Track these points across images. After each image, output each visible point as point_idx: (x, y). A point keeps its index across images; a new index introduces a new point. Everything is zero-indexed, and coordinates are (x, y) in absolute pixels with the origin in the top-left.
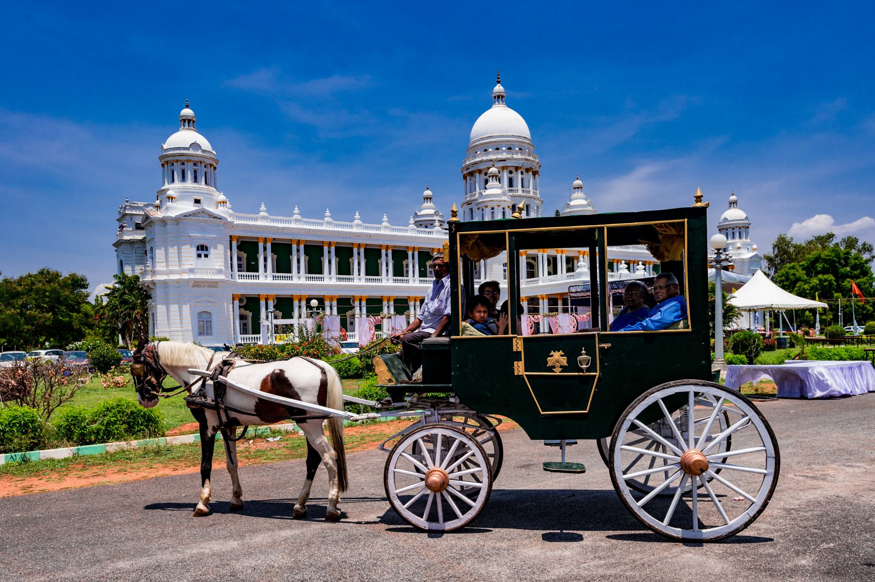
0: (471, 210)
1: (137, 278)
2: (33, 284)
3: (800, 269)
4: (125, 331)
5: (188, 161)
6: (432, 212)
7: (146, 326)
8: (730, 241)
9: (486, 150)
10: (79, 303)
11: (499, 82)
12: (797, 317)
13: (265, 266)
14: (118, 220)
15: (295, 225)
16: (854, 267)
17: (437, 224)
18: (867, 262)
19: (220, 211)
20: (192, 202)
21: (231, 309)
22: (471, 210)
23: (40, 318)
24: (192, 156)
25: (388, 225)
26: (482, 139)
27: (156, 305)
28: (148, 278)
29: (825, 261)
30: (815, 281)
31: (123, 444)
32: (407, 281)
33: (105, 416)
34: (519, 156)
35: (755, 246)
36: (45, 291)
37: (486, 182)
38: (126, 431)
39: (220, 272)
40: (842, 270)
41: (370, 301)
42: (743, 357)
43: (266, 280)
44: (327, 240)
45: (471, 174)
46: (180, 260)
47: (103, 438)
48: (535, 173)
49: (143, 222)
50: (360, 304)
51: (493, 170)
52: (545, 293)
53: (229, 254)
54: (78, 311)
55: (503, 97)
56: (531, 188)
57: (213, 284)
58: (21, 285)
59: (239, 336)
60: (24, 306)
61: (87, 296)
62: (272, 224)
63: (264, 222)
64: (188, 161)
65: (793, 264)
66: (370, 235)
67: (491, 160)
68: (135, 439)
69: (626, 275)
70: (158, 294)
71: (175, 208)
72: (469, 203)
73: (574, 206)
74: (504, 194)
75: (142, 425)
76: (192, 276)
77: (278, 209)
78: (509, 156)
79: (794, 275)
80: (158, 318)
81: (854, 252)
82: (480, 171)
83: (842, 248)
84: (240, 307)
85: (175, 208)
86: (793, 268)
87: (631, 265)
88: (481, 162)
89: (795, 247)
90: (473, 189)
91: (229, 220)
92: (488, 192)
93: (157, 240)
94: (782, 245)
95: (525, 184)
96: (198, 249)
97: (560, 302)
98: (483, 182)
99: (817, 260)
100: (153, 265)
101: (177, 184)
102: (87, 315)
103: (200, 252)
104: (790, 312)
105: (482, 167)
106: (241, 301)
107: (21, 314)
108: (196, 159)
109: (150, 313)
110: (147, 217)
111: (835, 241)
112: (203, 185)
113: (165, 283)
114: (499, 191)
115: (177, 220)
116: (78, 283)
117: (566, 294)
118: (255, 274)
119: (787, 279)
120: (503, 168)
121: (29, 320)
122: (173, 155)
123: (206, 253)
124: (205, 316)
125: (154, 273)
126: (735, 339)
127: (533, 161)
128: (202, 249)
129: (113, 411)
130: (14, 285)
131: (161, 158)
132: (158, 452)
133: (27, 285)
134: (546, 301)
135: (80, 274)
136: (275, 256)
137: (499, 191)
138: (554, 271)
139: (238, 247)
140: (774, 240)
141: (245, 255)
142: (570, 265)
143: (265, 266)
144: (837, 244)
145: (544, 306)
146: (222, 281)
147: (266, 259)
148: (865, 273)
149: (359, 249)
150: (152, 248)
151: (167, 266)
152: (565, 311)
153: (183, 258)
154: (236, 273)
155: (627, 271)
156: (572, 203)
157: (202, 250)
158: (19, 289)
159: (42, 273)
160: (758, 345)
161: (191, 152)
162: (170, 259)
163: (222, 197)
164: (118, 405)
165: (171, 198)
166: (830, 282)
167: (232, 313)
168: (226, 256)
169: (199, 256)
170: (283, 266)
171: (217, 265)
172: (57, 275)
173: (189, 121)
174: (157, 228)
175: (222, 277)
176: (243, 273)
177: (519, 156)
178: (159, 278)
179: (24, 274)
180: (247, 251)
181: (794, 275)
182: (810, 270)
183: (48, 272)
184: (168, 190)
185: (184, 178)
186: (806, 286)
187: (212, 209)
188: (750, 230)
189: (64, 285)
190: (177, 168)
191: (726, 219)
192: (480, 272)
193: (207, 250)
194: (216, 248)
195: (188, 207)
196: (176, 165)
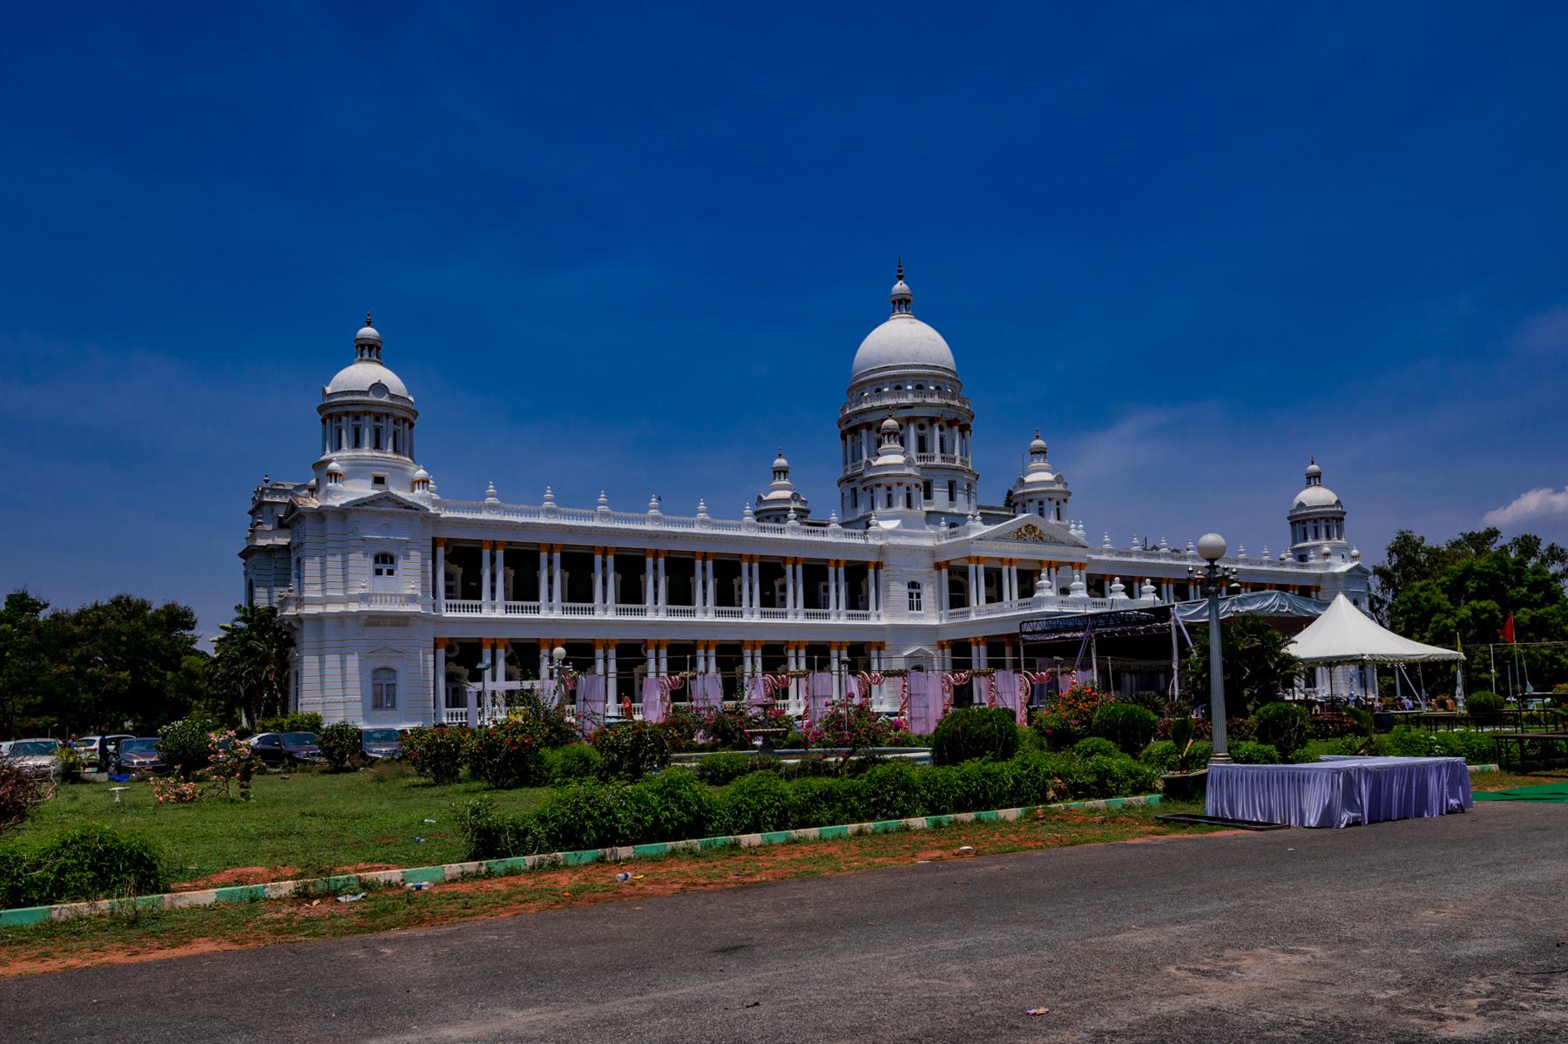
0: (854, 490)
1: (273, 611)
2: (101, 621)
3: (1438, 591)
4: (249, 703)
5: (366, 413)
6: (787, 494)
7: (286, 694)
8: (1310, 543)
9: (878, 390)
10: (178, 656)
11: (900, 278)
12: (1431, 676)
13: (493, 590)
14: (251, 513)
15: (545, 517)
16: (1535, 587)
17: (792, 514)
18: (1555, 578)
19: (417, 496)
20: (370, 482)
21: (431, 664)
22: (854, 490)
23: (109, 680)
24: (372, 404)
25: (497, 501)
26: (873, 371)
27: (301, 657)
28: (291, 611)
29: (1481, 575)
30: (1464, 611)
31: (83, 906)
32: (537, 610)
33: (58, 855)
34: (936, 400)
35: (1355, 552)
36: (120, 633)
37: (879, 443)
38: (92, 883)
39: (412, 599)
40: (1512, 593)
41: (571, 647)
42: (1270, 748)
43: (493, 611)
44: (833, 557)
45: (855, 431)
46: (345, 582)
47: (49, 895)
48: (964, 429)
49: (287, 516)
50: (657, 654)
51: (890, 423)
52: (980, 633)
53: (430, 569)
54: (176, 668)
55: (908, 301)
56: (957, 453)
57: (401, 620)
58: (79, 624)
59: (445, 710)
60: (84, 660)
61: (193, 641)
62: (506, 518)
63: (491, 513)
64: (366, 413)
65: (1424, 582)
66: (675, 536)
67: (887, 407)
68: (107, 897)
69: (1124, 602)
70: (307, 637)
71: (341, 492)
72: (849, 479)
73: (1033, 484)
74: (909, 463)
75: (125, 870)
76: (364, 607)
77: (518, 491)
78: (918, 400)
79: (1428, 600)
80: (306, 680)
81: (1532, 562)
82: (869, 426)
83: (1512, 555)
84: (447, 660)
85: (341, 492)
86: (1423, 589)
87: (1164, 586)
88: (871, 409)
89: (1429, 552)
90: (856, 456)
91: (432, 510)
92: (881, 461)
93: (307, 546)
94: (1405, 547)
95: (947, 446)
96: (377, 561)
97: (1008, 650)
98: (874, 444)
99: (1468, 572)
100: (301, 591)
101: (347, 453)
102: (190, 675)
103: (379, 566)
104: (1411, 666)
105: (871, 418)
106: (449, 649)
107: (78, 674)
108: (380, 410)
109: (292, 671)
110: (292, 508)
111: (1500, 543)
112: (389, 454)
113: (319, 618)
114: (899, 459)
115: (344, 512)
116: (178, 619)
117: (1016, 635)
118: (475, 602)
119: (1416, 608)
120: (909, 420)
121: (93, 683)
122: (342, 404)
123: (389, 566)
124: (385, 675)
125: (300, 602)
126: (1261, 718)
127: (959, 408)
128: (384, 562)
129: (75, 847)
130: (69, 625)
131: (321, 409)
132: (134, 921)
133: (91, 623)
134: (983, 648)
135: (182, 604)
136: (512, 573)
137: (899, 459)
138: (995, 596)
139: (446, 557)
140: (1391, 539)
141: (460, 571)
142: (1027, 586)
143: (493, 590)
144: (1504, 548)
145: (979, 657)
146: (416, 615)
147: (494, 576)
148: (1553, 597)
149: (704, 563)
150: (299, 561)
151: (324, 590)
152: (1016, 667)
153: (350, 577)
154: (442, 601)
155: (1124, 596)
156: (1028, 479)
157: (385, 562)
158: (77, 630)
159: (117, 602)
160: (1302, 727)
161: (372, 398)
162: (329, 578)
163: (421, 473)
164: (82, 837)
165: (334, 476)
166: (1491, 612)
167: (431, 671)
168: (424, 572)
169: (379, 572)
170: (680, 595)
171: (407, 590)
172: (143, 606)
173: (371, 347)
174: (309, 527)
175: (417, 608)
176: (453, 602)
177: (936, 400)
178: (310, 610)
179: (88, 606)
180: (462, 564)
181: (1428, 600)
182: (1456, 591)
183: (128, 601)
184: (330, 461)
185: (377, 445)
186: (1449, 622)
187: (403, 494)
188: (1347, 523)
189: (154, 623)
190: (1310, 526)
191: (1301, 505)
192: (867, 597)
193: (392, 562)
194: (407, 557)
195: (363, 489)
196: (348, 419)
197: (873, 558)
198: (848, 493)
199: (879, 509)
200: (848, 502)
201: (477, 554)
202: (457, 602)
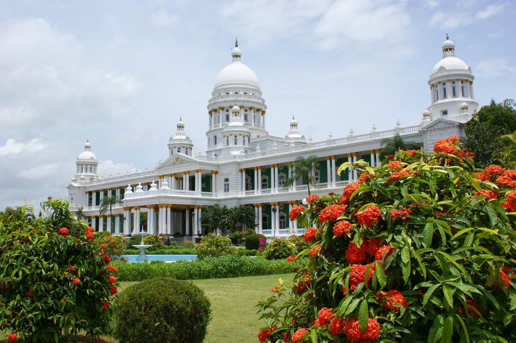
197: (215, 169)
198: (212, 138)
199: (231, 145)
200: (213, 142)
201: (369, 156)
202: (301, 186)
